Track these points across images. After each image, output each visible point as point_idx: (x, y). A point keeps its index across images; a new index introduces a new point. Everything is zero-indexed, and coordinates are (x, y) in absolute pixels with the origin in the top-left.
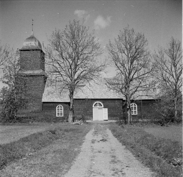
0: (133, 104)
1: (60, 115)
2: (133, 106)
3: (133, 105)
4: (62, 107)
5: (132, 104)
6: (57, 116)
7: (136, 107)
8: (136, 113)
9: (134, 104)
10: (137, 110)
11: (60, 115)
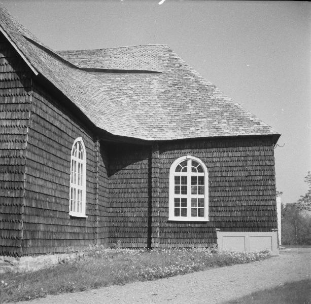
2: (189, 174)
3: (189, 166)
5: (185, 163)
6: (172, 217)
7: (202, 179)
8: (201, 214)
9: (194, 163)
11: (189, 212)
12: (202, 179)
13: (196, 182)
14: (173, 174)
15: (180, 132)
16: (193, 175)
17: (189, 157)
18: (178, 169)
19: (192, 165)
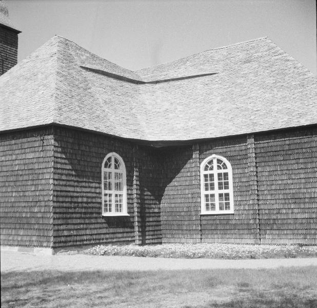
0: (215, 162)
1: (217, 206)
2: (215, 172)
3: (215, 164)
4: (225, 167)
5: (211, 162)
6: (204, 211)
7: (226, 174)
8: (227, 206)
9: (219, 161)
10: (230, 191)
11: (217, 206)
12: (226, 174)
13: (222, 187)
14: (203, 172)
15: (228, 124)
16: (218, 188)
17: (214, 156)
18: (206, 168)
19: (218, 163)
